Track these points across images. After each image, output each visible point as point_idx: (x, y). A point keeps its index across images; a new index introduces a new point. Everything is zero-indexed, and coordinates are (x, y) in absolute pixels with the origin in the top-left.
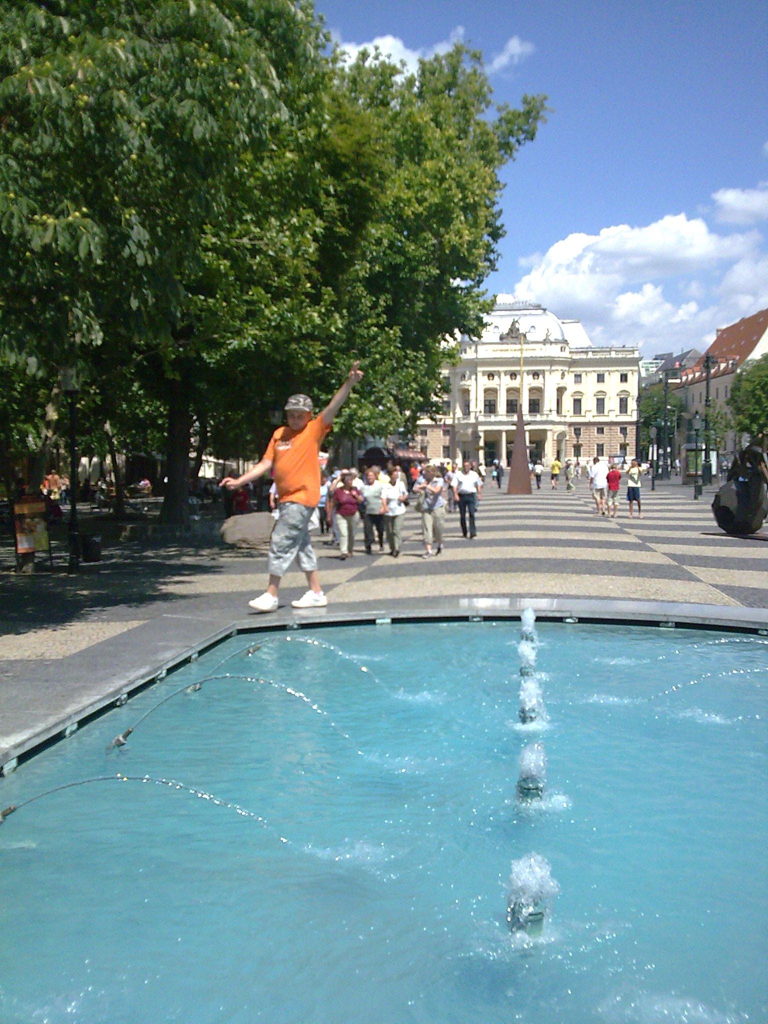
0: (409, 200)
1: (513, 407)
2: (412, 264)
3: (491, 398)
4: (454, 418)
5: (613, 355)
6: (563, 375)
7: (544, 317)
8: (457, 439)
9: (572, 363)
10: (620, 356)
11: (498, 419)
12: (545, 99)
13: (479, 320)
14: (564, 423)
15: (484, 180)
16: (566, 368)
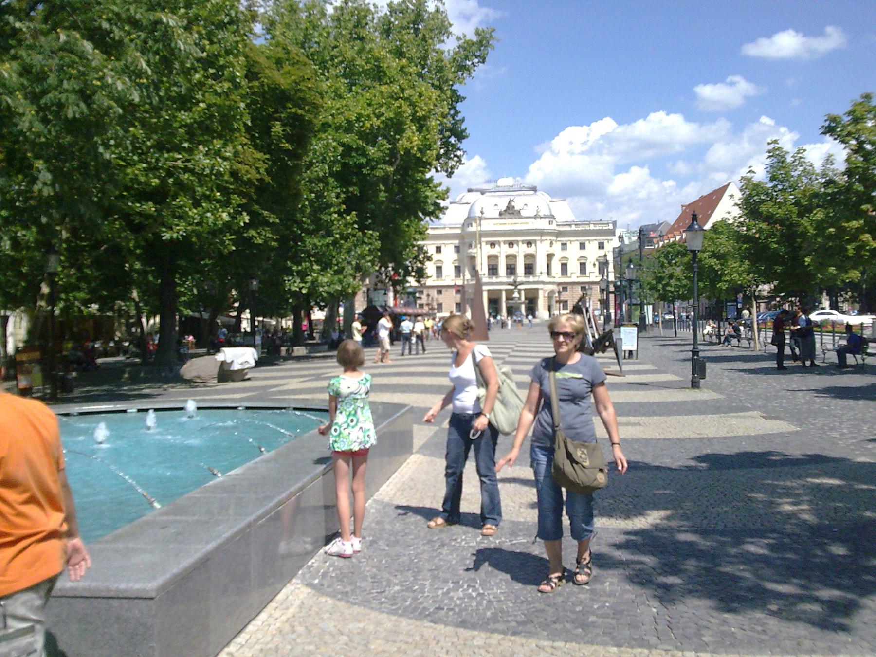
0: (368, 116)
1: (511, 270)
2: (372, 164)
3: (493, 263)
4: (464, 280)
5: (592, 227)
6: (551, 243)
7: (535, 196)
8: (467, 297)
9: (559, 234)
10: (597, 228)
11: (499, 280)
12: (493, 30)
13: (437, 205)
14: (553, 283)
15: (430, 99)
16: (554, 238)
